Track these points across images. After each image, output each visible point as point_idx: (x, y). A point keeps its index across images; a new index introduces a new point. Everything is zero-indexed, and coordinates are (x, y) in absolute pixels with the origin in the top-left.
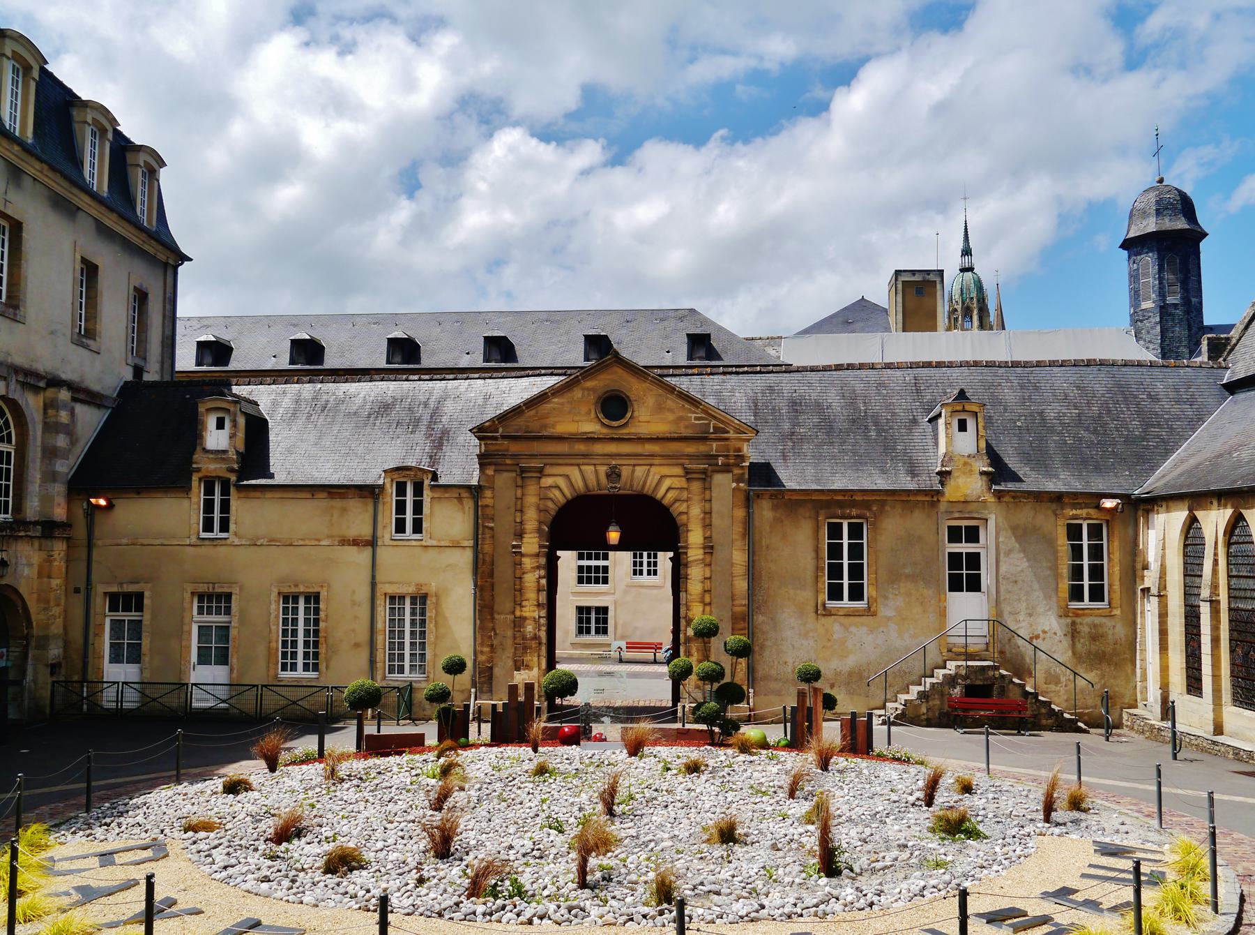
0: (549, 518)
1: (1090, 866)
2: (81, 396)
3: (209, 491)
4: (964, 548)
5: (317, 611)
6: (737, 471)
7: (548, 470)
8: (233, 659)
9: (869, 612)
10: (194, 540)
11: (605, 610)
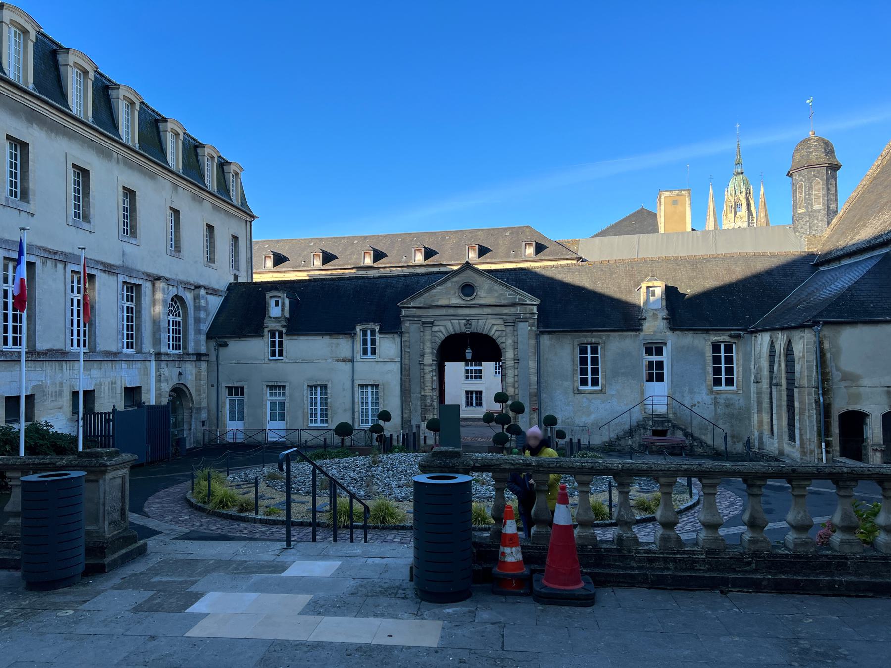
0: (437, 347)
1: (425, 437)
2: (210, 292)
3: (273, 336)
4: (655, 358)
5: (326, 393)
6: (530, 321)
7: (436, 323)
8: (287, 417)
9: (602, 392)
10: (267, 361)
11: (480, 393)
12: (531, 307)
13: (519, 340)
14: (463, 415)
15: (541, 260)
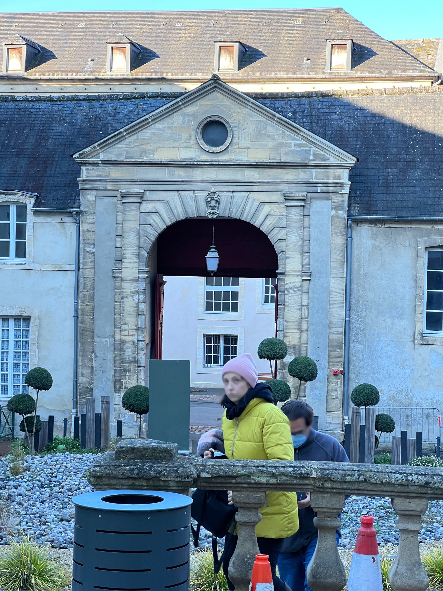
1: (119, 424)
6: (336, 198)
11: (233, 339)
12: (338, 172)
13: (308, 234)
14: (195, 382)
15: (362, 79)
